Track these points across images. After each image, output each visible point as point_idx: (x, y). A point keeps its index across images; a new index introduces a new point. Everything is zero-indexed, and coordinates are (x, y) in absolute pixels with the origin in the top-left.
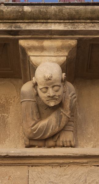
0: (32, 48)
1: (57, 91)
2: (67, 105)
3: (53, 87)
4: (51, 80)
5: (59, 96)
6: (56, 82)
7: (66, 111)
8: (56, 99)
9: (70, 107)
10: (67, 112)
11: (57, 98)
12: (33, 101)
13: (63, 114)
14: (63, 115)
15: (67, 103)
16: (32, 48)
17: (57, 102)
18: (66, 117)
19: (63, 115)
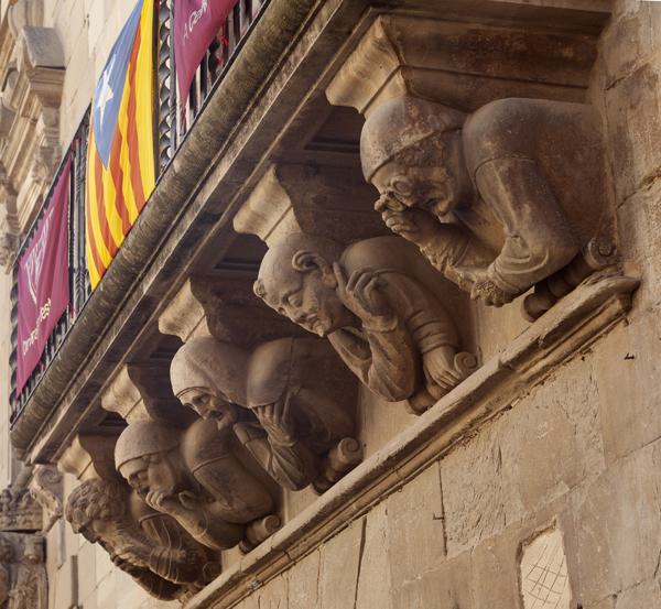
2: (360, 311)
5: (313, 310)
9: (367, 308)
11: (313, 315)
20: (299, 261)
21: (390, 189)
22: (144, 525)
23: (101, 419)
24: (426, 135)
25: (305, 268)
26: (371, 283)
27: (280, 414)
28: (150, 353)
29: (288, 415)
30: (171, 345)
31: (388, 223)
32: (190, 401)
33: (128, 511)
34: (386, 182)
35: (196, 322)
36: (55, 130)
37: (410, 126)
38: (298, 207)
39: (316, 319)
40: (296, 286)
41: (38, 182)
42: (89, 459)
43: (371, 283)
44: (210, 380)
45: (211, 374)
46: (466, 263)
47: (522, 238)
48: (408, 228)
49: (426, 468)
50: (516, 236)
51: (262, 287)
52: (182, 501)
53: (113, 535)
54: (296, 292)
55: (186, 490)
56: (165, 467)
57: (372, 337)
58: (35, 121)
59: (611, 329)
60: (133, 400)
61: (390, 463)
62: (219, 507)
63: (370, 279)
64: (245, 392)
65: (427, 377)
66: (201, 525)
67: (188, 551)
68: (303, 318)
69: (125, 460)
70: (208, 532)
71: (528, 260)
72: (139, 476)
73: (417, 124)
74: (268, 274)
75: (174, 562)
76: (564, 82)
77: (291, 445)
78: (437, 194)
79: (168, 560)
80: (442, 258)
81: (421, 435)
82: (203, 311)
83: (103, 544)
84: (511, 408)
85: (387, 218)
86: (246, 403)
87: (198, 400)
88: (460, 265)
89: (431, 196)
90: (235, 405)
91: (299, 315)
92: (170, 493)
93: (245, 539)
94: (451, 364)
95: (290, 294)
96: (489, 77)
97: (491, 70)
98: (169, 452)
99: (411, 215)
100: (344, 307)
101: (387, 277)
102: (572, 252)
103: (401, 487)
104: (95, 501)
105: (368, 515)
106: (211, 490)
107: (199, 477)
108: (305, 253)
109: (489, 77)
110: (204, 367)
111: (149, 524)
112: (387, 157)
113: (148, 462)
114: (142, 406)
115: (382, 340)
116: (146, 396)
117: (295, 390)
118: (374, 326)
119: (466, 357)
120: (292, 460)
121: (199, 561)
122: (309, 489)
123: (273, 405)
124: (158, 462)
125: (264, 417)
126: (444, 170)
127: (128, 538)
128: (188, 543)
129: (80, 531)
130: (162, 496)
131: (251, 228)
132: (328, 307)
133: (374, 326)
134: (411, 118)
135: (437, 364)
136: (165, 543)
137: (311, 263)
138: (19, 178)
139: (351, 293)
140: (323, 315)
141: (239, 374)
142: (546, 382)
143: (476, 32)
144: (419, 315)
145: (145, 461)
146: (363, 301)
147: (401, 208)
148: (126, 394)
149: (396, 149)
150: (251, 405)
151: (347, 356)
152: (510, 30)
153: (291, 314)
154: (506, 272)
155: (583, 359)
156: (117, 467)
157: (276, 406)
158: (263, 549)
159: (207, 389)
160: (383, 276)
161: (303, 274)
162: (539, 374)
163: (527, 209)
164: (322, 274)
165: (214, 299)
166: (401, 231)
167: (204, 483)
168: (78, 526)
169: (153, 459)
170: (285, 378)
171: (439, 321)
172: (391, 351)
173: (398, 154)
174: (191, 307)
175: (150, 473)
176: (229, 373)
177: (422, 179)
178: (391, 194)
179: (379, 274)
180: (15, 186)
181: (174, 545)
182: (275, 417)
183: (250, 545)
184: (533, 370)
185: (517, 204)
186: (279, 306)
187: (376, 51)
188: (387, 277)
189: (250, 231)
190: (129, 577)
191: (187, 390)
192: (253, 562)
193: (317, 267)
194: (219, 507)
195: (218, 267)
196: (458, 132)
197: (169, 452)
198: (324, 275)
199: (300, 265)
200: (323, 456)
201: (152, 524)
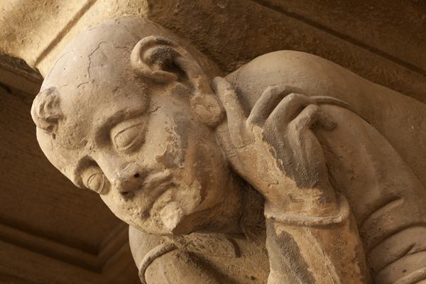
0: (16, 27)
1: (136, 145)
2: (267, 171)
3: (104, 138)
4: (61, 117)
5: (165, 161)
6: (93, 111)
7: (291, 205)
8: (169, 183)
9: (289, 168)
10: (300, 205)
11: (166, 173)
12: (159, 255)
13: (287, 230)
14: (292, 232)
15: (259, 165)
16: (16, 27)
17: (183, 193)
18: (309, 233)
19: (292, 232)
26: (306, 113)
40: (134, 104)
43: (306, 113)
54: (134, 115)
63: (302, 108)
108: (160, 42)
132: (200, 157)
139: (257, 131)
146: (277, 143)
160: (326, 107)
179: (319, 103)
186: (83, 153)
188: (336, 113)
198: (197, 94)
199: (150, 62)
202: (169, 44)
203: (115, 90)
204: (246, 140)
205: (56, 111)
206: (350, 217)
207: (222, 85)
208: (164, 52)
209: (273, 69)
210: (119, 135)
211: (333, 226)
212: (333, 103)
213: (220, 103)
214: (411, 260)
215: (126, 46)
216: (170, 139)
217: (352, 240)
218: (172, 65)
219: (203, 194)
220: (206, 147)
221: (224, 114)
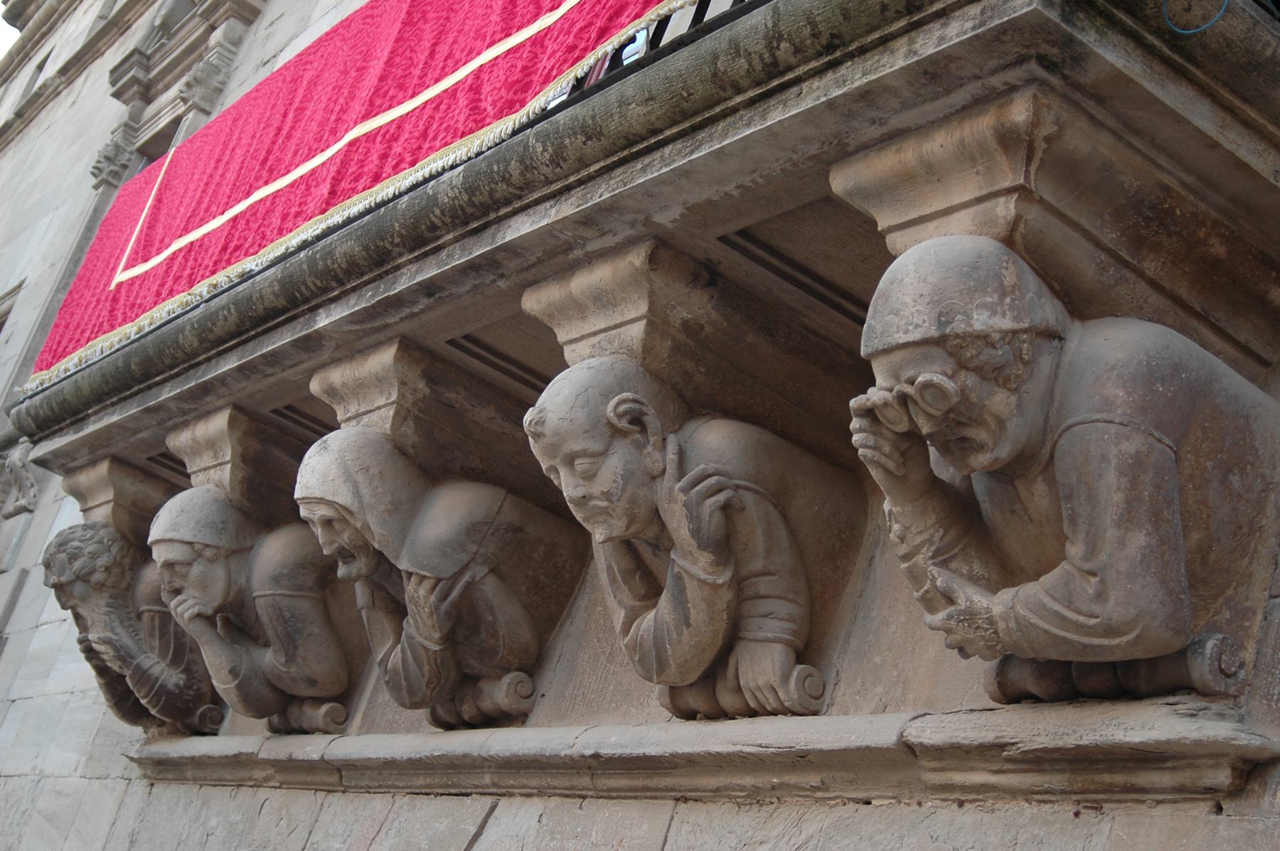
2: (679, 527)
5: (607, 495)
9: (695, 533)
11: (605, 504)
20: (622, 408)
21: (909, 390)
22: (146, 617)
23: (153, 453)
24: (1016, 326)
25: (624, 424)
26: (721, 497)
27: (444, 597)
28: (272, 407)
29: (454, 605)
30: (320, 424)
31: (856, 438)
32: (315, 518)
33: (131, 587)
34: (909, 373)
35: (376, 405)
36: (233, 49)
37: (996, 297)
38: (655, 322)
39: (605, 511)
40: (596, 446)
41: (184, 100)
42: (110, 495)
43: (721, 497)
44: (360, 502)
45: (365, 491)
46: (954, 565)
47: (1102, 582)
48: (891, 465)
49: (651, 798)
50: (1092, 573)
51: (540, 422)
52: (219, 624)
53: (97, 610)
54: (594, 455)
55: (236, 621)
56: (219, 573)
57: (678, 577)
58: (213, 28)
59: (1175, 802)
60: (216, 456)
61: (594, 762)
62: (269, 658)
63: (720, 490)
64: (402, 543)
65: (731, 672)
66: (234, 672)
67: (188, 679)
68: (583, 500)
69: (169, 536)
70: (238, 687)
71: (1093, 621)
72: (177, 568)
73: (1008, 300)
74: (556, 403)
75: (163, 687)
76: (1242, 337)
77: (437, 648)
78: (981, 435)
79: (157, 679)
80: (918, 540)
81: (675, 756)
82: (394, 397)
83: (78, 617)
84: (868, 803)
85: (861, 430)
86: (397, 558)
87: (328, 523)
88: (944, 564)
89: (971, 433)
90: (380, 554)
91: (579, 492)
92: (210, 611)
93: (283, 713)
94: (785, 678)
95: (584, 454)
96: (1140, 274)
97: (1150, 266)
98: (234, 552)
99: (905, 446)
100: (656, 512)
101: (749, 499)
102: (1178, 644)
103: (584, 797)
104: (94, 556)
105: (503, 802)
106: (270, 632)
107: (262, 608)
108: (635, 401)
109: (1140, 274)
110: (360, 478)
111: (152, 618)
112: (933, 332)
113: (200, 554)
114: (225, 473)
115: (692, 591)
116: (238, 461)
117: (479, 571)
118: (693, 565)
119: (809, 675)
120: (426, 668)
121: (198, 699)
122: (423, 713)
123: (439, 580)
124: (212, 561)
125: (417, 594)
126: (1013, 399)
127: (116, 624)
128: (194, 668)
129: (54, 586)
130: (196, 610)
131: (551, 316)
132: (633, 501)
133: (693, 565)
134: (1002, 284)
135: (762, 666)
136: (163, 654)
137: (637, 420)
138: (160, 86)
139: (682, 497)
140: (619, 511)
141: (406, 511)
142: (967, 806)
143: (1167, 190)
144: (772, 578)
145: (196, 551)
146: (692, 511)
147: (903, 427)
148: (211, 444)
149: (959, 326)
150: (403, 565)
151: (613, 581)
152: (1213, 214)
153: (569, 486)
154: (1034, 619)
155: (1077, 814)
156: (150, 540)
157: (442, 585)
158: (311, 748)
159: (351, 513)
160: (741, 492)
161: (616, 432)
162: (964, 788)
163: (1139, 540)
164: (645, 446)
165: (421, 385)
166: (872, 462)
167: (264, 619)
168: (54, 579)
169: (208, 553)
170: (474, 548)
171: (793, 601)
172: (697, 615)
173: (957, 336)
174: (379, 381)
175: (196, 570)
176: (392, 503)
177: (974, 398)
178: (903, 399)
179: (738, 487)
180: (153, 91)
181: (175, 662)
182: (433, 598)
183: (285, 729)
184: (959, 778)
185: (1127, 519)
186: (552, 463)
187: (992, 142)
188: (749, 499)
189: (546, 320)
190: (93, 673)
191: (321, 501)
192: (282, 755)
193: (644, 429)
194: (269, 658)
195: (451, 342)
196: (1056, 342)
197: (234, 552)
198: (650, 448)
199: (620, 416)
200: (469, 681)
201: (157, 622)
202: (642, 404)
203: (586, 432)
204: (671, 500)
205: (539, 429)
206: (731, 580)
207: (672, 439)
208: (633, 411)
209: (716, 440)
210: (581, 465)
211: (715, 587)
212: (748, 489)
213: (664, 460)
214: (768, 621)
215: (606, 397)
216: (615, 481)
217: (727, 596)
218: (637, 420)
219: (628, 528)
220: (642, 493)
221: (665, 470)
